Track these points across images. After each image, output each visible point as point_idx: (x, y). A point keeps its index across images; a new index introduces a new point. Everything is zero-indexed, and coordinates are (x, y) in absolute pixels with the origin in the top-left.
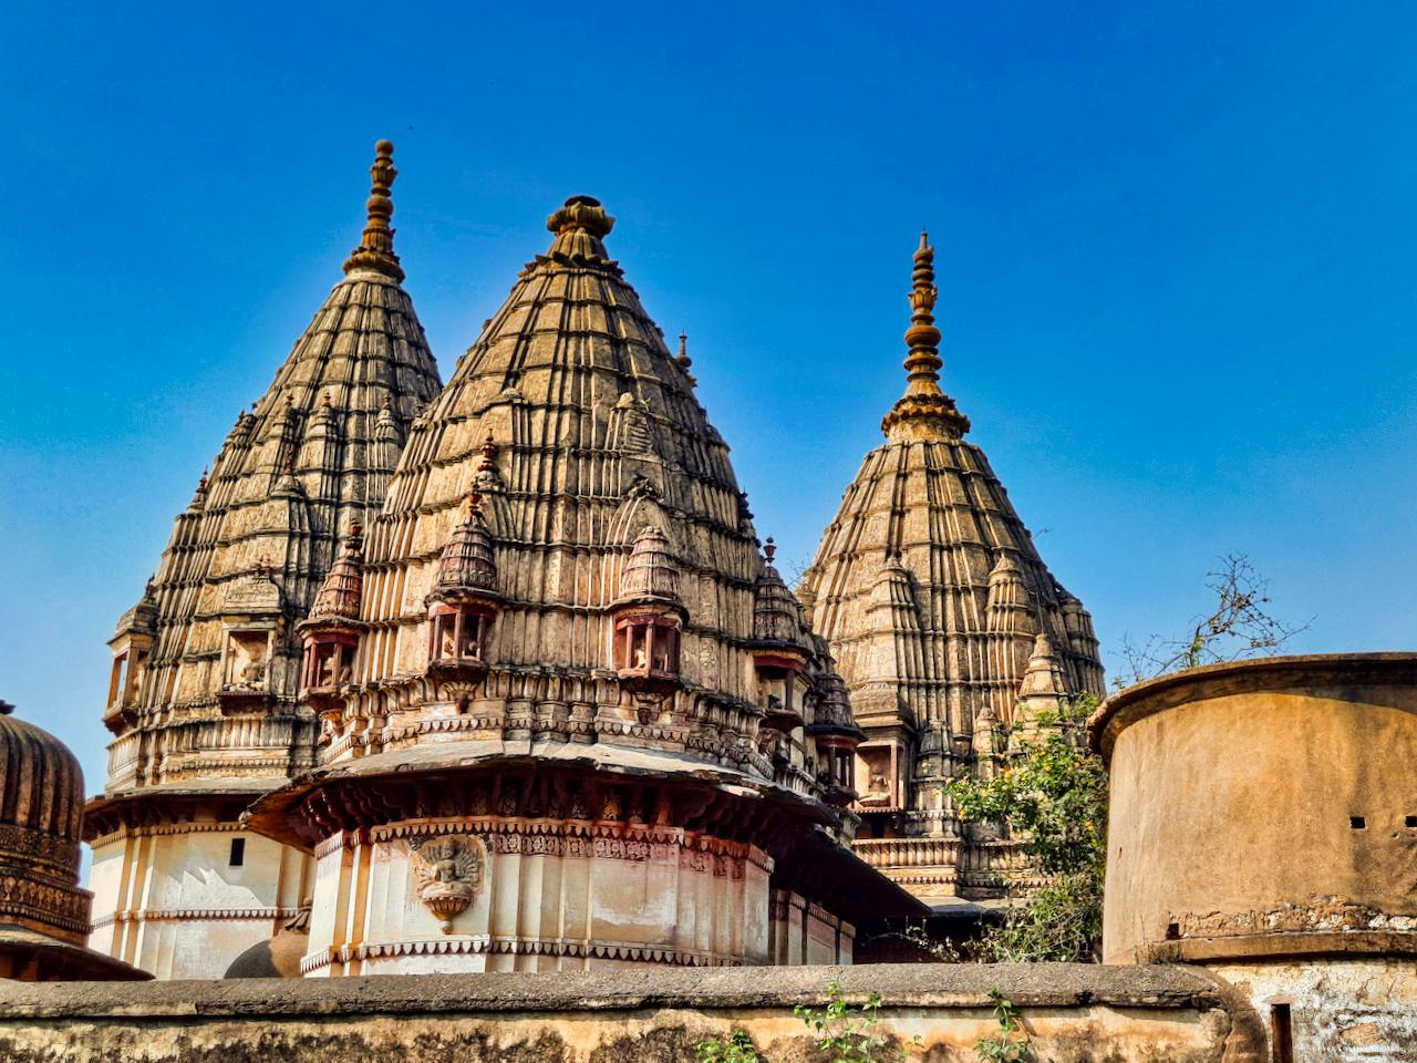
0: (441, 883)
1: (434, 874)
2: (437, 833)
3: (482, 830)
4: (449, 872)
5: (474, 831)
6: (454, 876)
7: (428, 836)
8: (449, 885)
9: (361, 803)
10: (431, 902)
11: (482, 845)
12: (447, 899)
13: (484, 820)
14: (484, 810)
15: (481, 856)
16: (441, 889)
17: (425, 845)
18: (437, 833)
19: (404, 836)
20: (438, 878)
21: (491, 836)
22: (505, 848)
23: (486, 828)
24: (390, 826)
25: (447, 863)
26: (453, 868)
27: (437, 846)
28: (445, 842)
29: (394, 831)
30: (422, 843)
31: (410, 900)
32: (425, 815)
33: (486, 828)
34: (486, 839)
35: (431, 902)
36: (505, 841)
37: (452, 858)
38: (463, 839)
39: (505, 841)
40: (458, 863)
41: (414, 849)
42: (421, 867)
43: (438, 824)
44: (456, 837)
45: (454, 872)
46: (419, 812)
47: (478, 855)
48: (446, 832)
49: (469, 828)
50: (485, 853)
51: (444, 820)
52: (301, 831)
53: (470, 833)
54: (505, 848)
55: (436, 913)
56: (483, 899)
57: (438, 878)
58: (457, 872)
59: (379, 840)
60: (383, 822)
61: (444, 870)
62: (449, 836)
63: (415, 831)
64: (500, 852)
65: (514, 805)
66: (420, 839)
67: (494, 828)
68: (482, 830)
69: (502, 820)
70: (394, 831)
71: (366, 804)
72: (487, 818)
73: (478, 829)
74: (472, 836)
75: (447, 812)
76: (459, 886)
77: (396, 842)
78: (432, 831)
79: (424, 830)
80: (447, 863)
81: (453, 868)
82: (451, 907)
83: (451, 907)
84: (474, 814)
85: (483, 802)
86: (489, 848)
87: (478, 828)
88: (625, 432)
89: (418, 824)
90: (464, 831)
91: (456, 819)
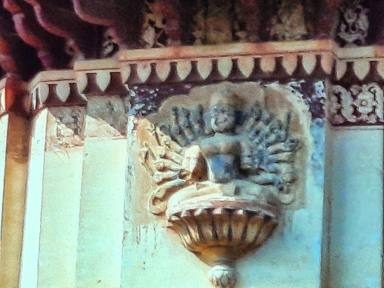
0: (210, 184)
1: (190, 166)
2: (194, 79)
3: (299, 72)
4: (228, 160)
5: (279, 75)
6: (238, 170)
7: (173, 86)
8: (231, 187)
9: (18, 19)
10: (181, 212)
11: (300, 105)
12: (230, 212)
13: (297, 48)
14: (301, 30)
15: (298, 128)
16: (213, 194)
17: (166, 105)
18: (194, 79)
19: (115, 87)
20: (200, 174)
21: (319, 85)
22: (347, 112)
23: (309, 66)
24: (81, 68)
25: (222, 142)
26: (235, 152)
27: (193, 107)
28: (216, 98)
29: (91, 78)
30: (158, 101)
31: (136, 220)
32: (162, 40)
33: (309, 66)
34: (307, 90)
35: (181, 212)
36: (346, 97)
37: (231, 130)
38: (254, 92)
39: (346, 97)
40: (245, 140)
41: (141, 114)
42: (159, 151)
43: (200, 57)
44: (237, 87)
45: (238, 160)
46: (149, 36)
47: (291, 123)
48: (214, 77)
49: (267, 66)
50: (305, 120)
51: (210, 50)
52: (84, 92)
53: (268, 79)
54: (347, 112)
55: (197, 249)
56: (307, 217)
57: (200, 174)
58: (246, 161)
59: (52, 101)
60: (63, 62)
61: (214, 154)
62: (223, 86)
63: (143, 75)
64: (338, 123)
65: (363, 23)
66: (159, 91)
67: (326, 67)
68: (299, 72)
69: (341, 53)
70: (91, 78)
71: (30, 22)
72: (312, 45)
73: (289, 67)
74: (274, 86)
75: (213, 35)
76: (252, 191)
77: (96, 103)
78: (183, 73)
79: (163, 74)
80: (222, 142)
81: (235, 152)
82: (237, 232)
83: (237, 232)
84: (275, 38)
85: (297, 15)
86: (316, 111)
87: (289, 67)
88: (313, 190)
89: (147, 59)
90: (257, 74)
91: (238, 48)
